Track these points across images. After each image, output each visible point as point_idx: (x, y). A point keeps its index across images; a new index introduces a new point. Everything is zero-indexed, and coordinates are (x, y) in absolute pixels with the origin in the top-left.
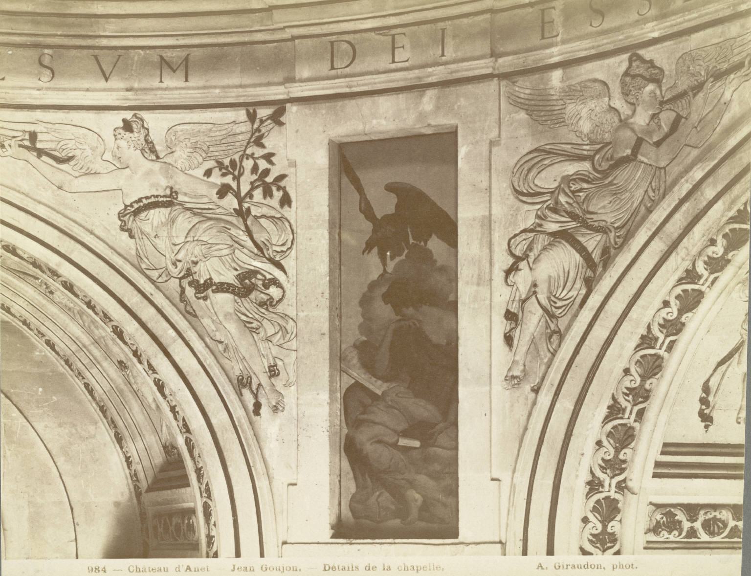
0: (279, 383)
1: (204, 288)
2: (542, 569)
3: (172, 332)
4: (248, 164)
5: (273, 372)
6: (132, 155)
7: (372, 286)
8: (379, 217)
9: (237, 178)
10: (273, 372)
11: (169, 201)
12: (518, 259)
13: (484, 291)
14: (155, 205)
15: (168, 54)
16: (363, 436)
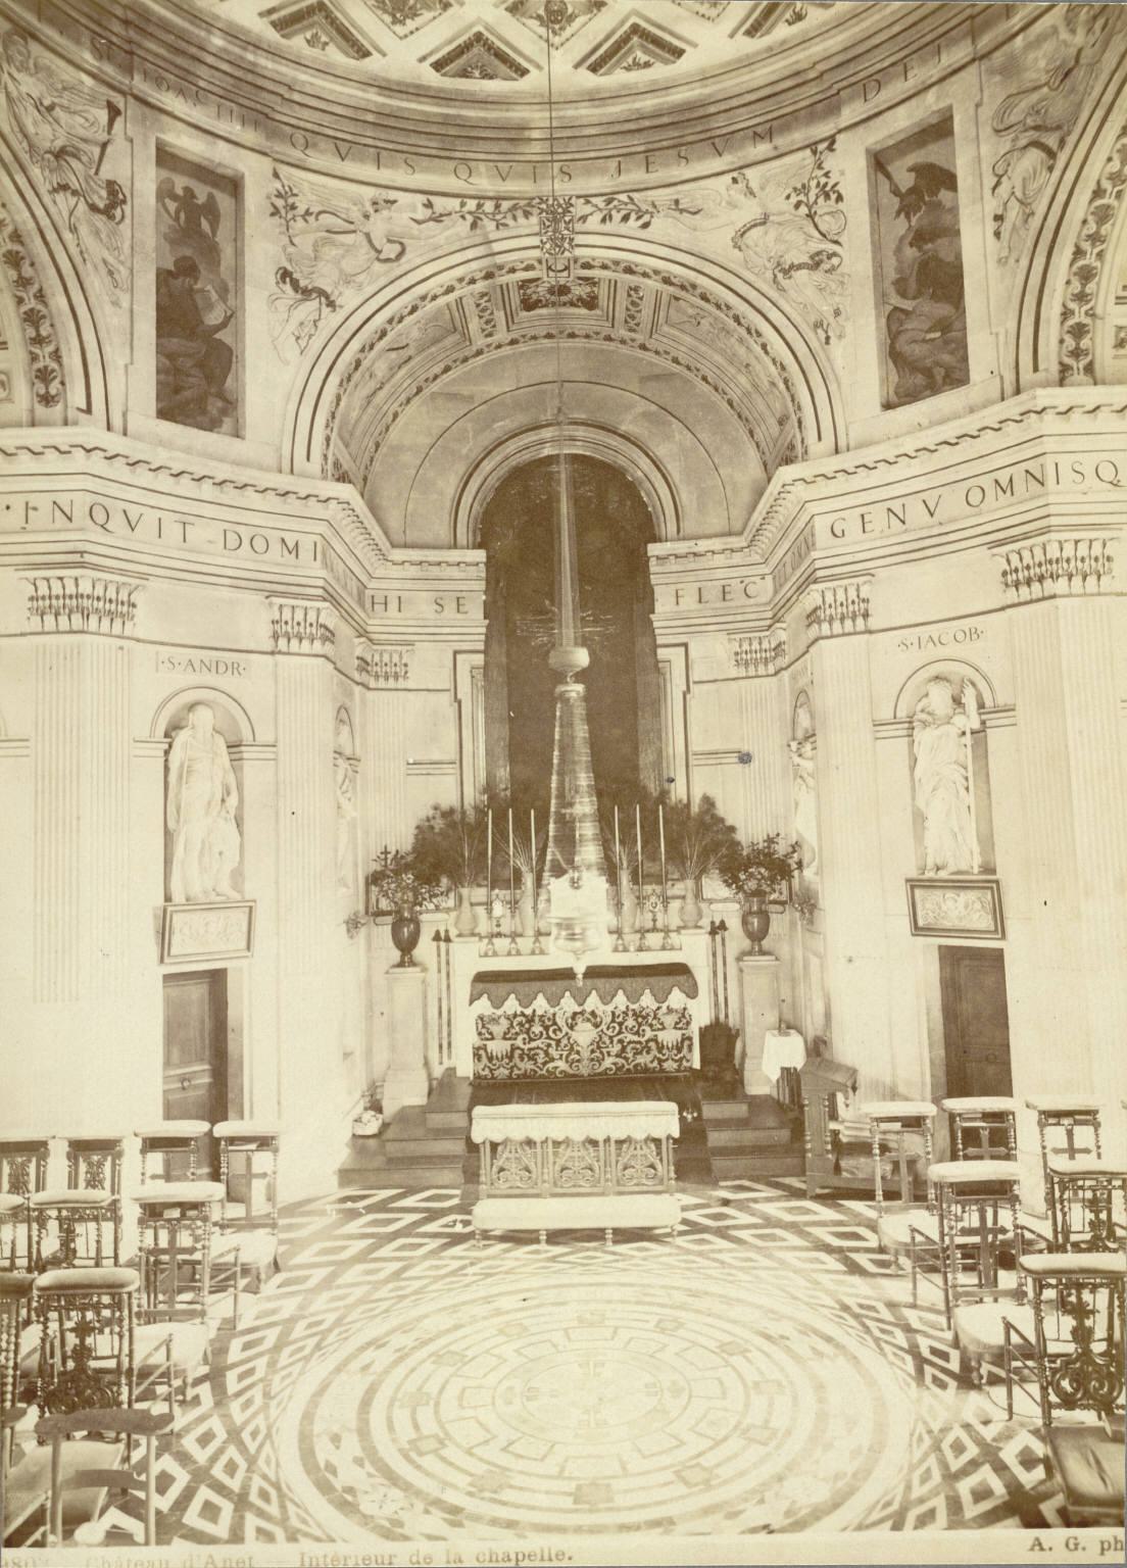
0: (840, 319)
1: (788, 271)
2: (1042, 1549)
3: (769, 304)
4: (813, 183)
5: (837, 313)
6: (740, 198)
7: (902, 239)
8: (903, 191)
9: (807, 195)
10: (837, 313)
11: (764, 221)
12: (1001, 177)
13: (978, 207)
14: (755, 226)
15: (759, 129)
16: (902, 345)
